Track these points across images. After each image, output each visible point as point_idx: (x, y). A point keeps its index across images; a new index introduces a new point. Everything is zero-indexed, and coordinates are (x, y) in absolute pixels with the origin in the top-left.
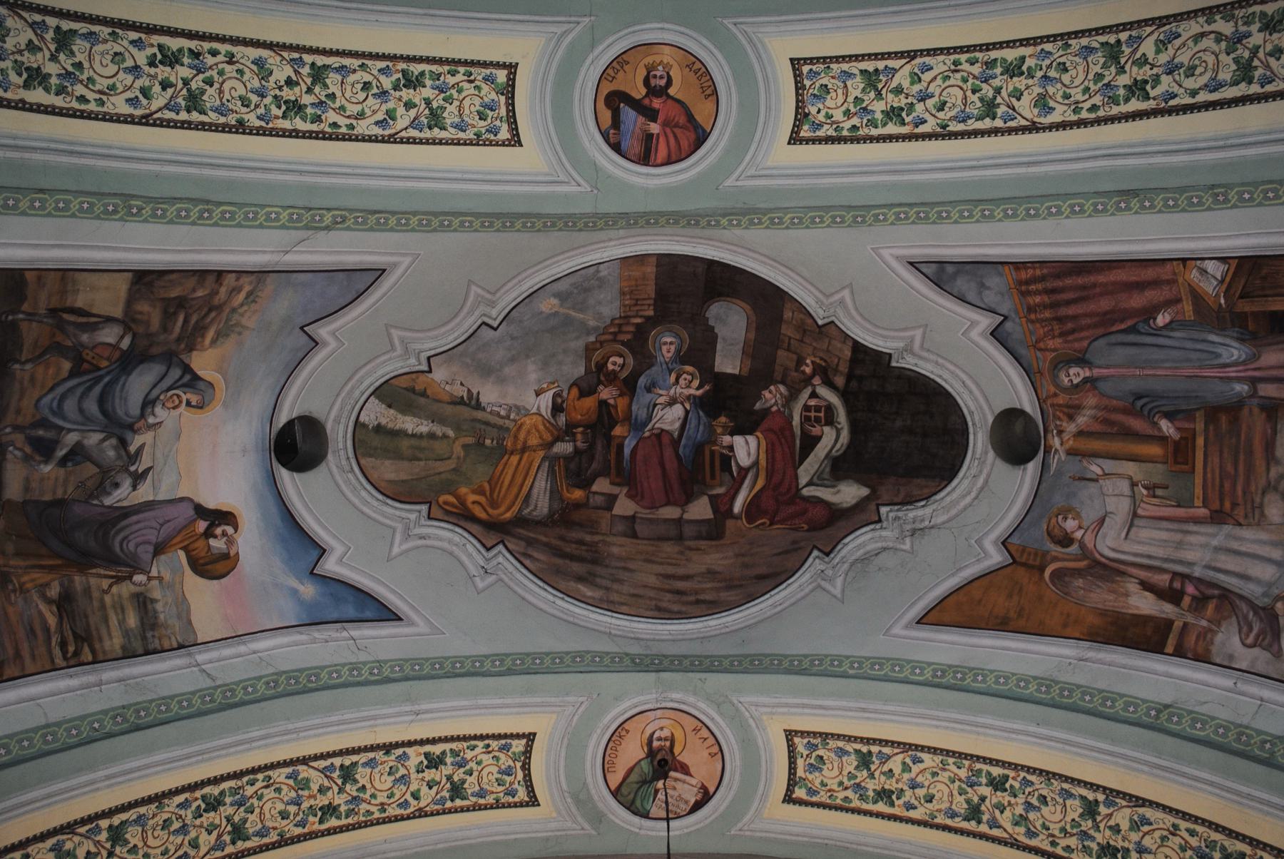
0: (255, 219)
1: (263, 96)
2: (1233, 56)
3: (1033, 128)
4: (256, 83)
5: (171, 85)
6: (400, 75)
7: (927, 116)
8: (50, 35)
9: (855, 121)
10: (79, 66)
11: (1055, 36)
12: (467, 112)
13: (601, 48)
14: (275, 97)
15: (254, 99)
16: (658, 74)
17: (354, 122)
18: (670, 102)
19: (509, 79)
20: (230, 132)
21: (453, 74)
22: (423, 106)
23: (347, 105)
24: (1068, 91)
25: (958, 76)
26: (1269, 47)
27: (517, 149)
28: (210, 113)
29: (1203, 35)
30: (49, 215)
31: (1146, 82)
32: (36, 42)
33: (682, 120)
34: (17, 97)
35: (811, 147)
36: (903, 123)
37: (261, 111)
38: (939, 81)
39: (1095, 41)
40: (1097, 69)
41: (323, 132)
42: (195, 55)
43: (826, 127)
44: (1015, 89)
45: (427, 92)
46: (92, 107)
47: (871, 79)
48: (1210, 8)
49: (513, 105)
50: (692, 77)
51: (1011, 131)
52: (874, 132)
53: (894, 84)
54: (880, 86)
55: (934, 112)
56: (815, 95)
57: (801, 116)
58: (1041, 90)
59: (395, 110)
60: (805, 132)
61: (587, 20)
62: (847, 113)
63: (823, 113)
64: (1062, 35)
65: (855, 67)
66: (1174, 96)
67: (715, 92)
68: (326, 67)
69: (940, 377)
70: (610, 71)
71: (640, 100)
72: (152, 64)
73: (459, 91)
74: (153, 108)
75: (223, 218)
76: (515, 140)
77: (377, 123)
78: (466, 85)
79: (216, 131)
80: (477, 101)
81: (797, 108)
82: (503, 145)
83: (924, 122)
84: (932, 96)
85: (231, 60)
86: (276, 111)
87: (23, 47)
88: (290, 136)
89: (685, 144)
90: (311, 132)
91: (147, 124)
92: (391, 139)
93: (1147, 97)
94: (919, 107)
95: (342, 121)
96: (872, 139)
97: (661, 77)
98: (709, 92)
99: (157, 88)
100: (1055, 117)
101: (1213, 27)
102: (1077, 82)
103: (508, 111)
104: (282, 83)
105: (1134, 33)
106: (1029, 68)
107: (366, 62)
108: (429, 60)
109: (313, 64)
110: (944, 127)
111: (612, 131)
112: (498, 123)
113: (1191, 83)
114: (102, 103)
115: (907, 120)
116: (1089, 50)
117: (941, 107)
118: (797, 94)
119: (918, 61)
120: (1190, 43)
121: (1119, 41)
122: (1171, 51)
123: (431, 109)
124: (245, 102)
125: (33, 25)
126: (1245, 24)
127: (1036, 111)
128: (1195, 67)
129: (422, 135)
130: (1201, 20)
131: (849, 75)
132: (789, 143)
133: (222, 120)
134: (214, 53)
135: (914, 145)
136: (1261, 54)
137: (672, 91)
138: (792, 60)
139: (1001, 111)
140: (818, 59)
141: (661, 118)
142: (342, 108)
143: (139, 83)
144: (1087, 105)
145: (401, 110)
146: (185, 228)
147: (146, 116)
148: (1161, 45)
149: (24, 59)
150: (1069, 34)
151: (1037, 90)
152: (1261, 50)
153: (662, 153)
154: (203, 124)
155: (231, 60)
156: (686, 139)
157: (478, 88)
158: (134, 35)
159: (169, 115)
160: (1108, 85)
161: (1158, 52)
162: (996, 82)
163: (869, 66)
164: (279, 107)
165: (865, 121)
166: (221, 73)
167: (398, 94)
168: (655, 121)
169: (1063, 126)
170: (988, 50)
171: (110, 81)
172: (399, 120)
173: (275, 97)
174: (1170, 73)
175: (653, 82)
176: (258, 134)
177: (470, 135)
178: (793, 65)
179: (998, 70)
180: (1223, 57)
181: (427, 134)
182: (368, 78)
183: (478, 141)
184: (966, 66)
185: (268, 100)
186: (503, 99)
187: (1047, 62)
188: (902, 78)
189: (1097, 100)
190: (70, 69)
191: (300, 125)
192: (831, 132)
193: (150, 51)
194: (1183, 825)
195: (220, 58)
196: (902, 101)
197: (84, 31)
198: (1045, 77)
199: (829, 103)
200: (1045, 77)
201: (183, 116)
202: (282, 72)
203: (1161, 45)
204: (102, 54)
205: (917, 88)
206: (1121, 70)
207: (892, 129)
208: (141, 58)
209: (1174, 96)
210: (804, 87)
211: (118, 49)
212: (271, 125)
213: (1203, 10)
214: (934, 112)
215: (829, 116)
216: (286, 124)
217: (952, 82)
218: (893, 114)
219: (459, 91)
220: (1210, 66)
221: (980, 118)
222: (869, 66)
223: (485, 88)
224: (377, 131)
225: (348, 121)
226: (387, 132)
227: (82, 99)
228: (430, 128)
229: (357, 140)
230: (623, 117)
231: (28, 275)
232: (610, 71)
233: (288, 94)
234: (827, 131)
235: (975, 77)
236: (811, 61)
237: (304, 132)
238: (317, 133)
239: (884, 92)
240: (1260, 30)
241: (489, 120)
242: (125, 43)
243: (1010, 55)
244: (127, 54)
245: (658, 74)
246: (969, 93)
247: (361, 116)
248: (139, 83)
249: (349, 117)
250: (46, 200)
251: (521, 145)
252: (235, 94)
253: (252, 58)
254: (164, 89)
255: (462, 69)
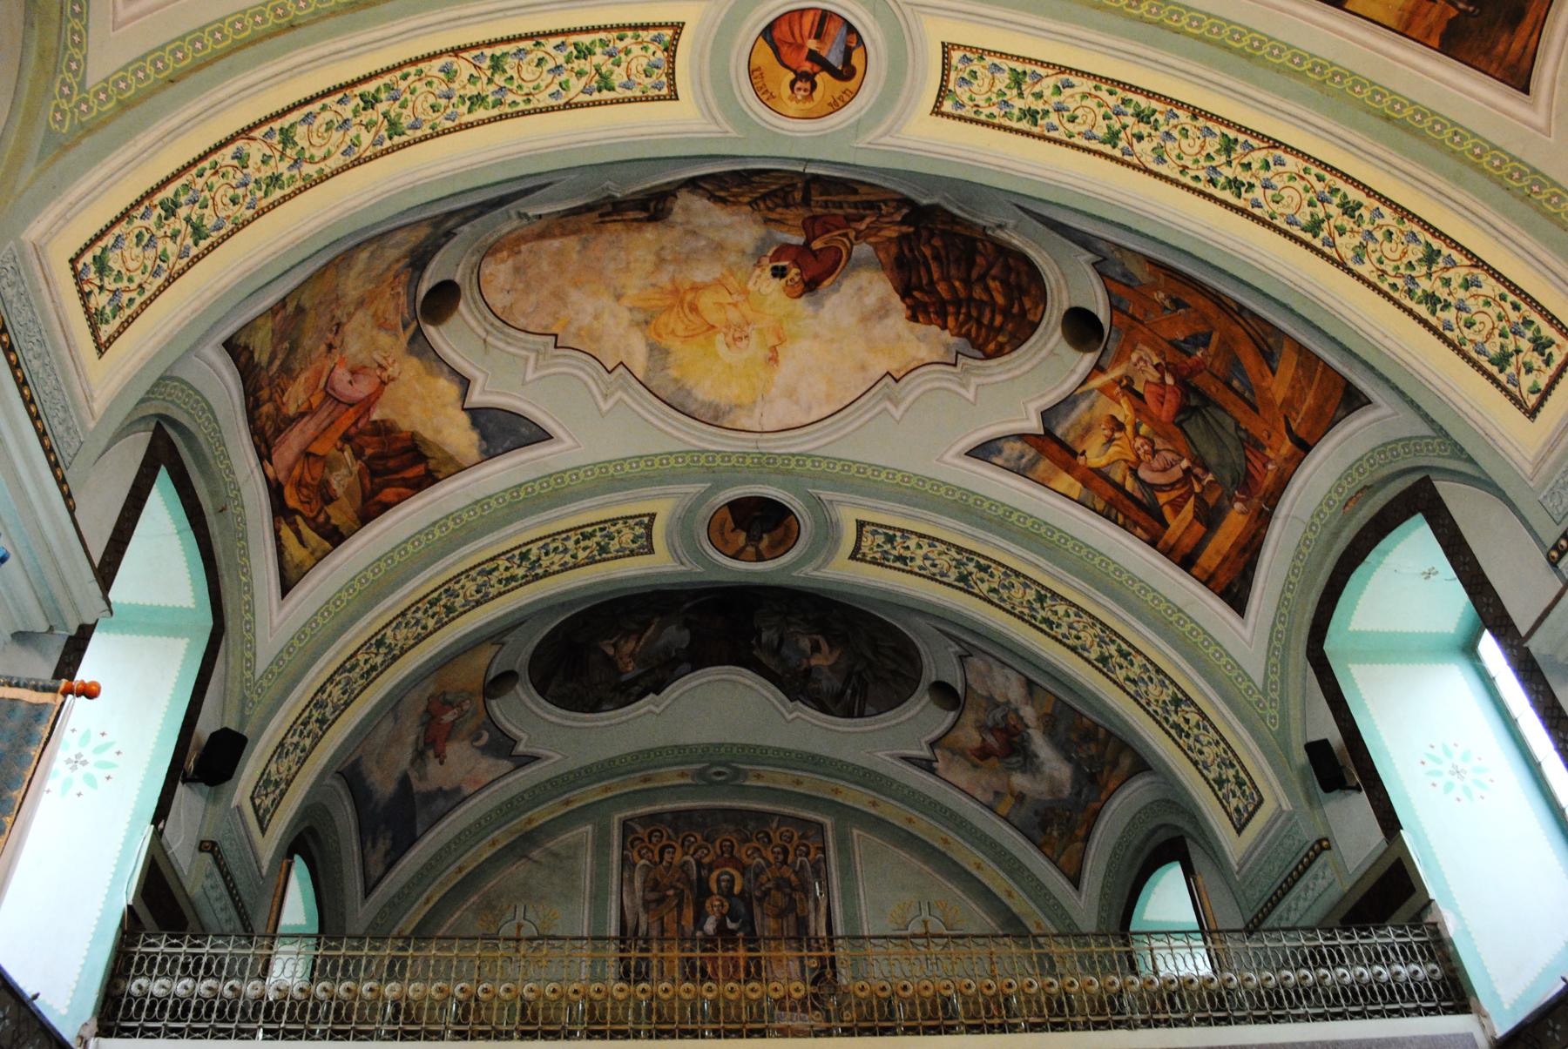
0: (1213, 25)
1: (1168, 134)
2: (299, 148)
3: (456, 51)
4: (1169, 145)
5: (1243, 165)
6: (1040, 122)
7: (553, 52)
8: (1323, 234)
9: (620, 45)
10: (1311, 204)
11: (444, 134)
12: (987, 81)
13: (852, 120)
14: (1156, 129)
15: (1175, 133)
16: (802, 92)
17: (1093, 92)
18: (794, 67)
19: (941, 103)
20: (1207, 112)
21: (992, 115)
22: (1025, 94)
23: (1095, 108)
24: (429, 89)
25: (526, 90)
26: (272, 162)
27: (946, 40)
28: (1218, 133)
29: (325, 158)
30: (1392, 93)
31: (364, 109)
32: (1336, 234)
33: (784, 49)
34: (1372, 200)
35: (663, 20)
36: (576, 45)
37: (1173, 122)
38: (543, 85)
39: (411, 135)
40: (405, 112)
41: (1124, 89)
42: (1212, 182)
43: (648, 39)
44: (474, 84)
45: (1019, 104)
46: (1314, 170)
47: (605, 84)
48: (322, 181)
49: (942, 79)
50: (770, 86)
51: (477, 46)
52: (602, 35)
53: (584, 80)
54: (597, 77)
55: (547, 57)
56: (657, 67)
57: (671, 49)
58: (451, 85)
59: (1053, 94)
60: (667, 34)
61: (860, 145)
62: (627, 52)
63: (650, 51)
64: (438, 135)
65: (620, 93)
66: (340, 102)
67: (750, 73)
68: (1104, 142)
69: (1048, 323)
70: (847, 99)
71: (822, 70)
72: (1251, 186)
73: (989, 99)
74: (1265, 152)
75: (1242, 35)
76: (947, 48)
77: (1072, 86)
78: (982, 103)
79: (1218, 117)
80: (975, 88)
81: (674, 57)
82: (959, 46)
83: (557, 47)
84: (550, 71)
85: (1184, 169)
86: (1161, 118)
87: (1348, 234)
88: (1155, 94)
89: (785, 28)
90: (1135, 92)
91: (1276, 141)
92: (1063, 69)
93: (362, 96)
94: (561, 60)
95: (1104, 95)
96: (605, 29)
97: (799, 89)
98: (756, 73)
99: (1255, 166)
100: (438, 63)
101: (317, 167)
102: (421, 98)
103: (948, 76)
104: (1146, 139)
105: (379, 148)
106: (464, 103)
107: (1067, 139)
108: (1011, 130)
109: (1114, 147)
110: (538, 44)
111: (853, 45)
112: (960, 66)
113: (328, 116)
114: (1305, 170)
115: (572, 48)
116: (414, 127)
117: (540, 61)
118: (673, 69)
119: (562, 101)
120: (333, 149)
121: (390, 138)
122: (348, 139)
123: (1019, 88)
124: (1185, 133)
125: (1333, 245)
126: (293, 177)
127: (455, 67)
128: (327, 130)
129: (1034, 68)
130: (327, 171)
131: (626, 86)
132: (683, 24)
133: (1210, 124)
134: (1197, 178)
135: (565, 26)
136: (277, 155)
137: (792, 76)
138: (677, 99)
139: (486, 64)
140: (653, 100)
141: (805, 52)
142: (1100, 105)
143: (1268, 175)
144: (412, 78)
145: (1047, 93)
146: (1280, 37)
147: (1274, 147)
148: (355, 143)
149: (1352, 225)
150: (432, 137)
151: (455, 86)
152: (278, 158)
153: (808, 20)
154: (1228, 126)
155: (1184, 169)
156: (782, 32)
157: (971, 99)
158: (1257, 211)
159: (1254, 142)
160: (395, 99)
161: (358, 137)
162: (492, 88)
163: (606, 95)
164: (1156, 121)
165: (611, 45)
166: (1197, 161)
167: (1046, 107)
168: (810, 51)
169: (430, 57)
170: (501, 116)
171: (1292, 184)
172: (1051, 86)
173: (1156, 129)
174: (346, 121)
175: (808, 85)
176: (1183, 103)
177: (989, 60)
178: (676, 95)
179: (491, 99)
180: (305, 144)
181: (1029, 68)
182: (1070, 126)
183: (982, 53)
184: (519, 99)
185: (1163, 129)
186: (951, 87)
187: (448, 111)
188: (576, 85)
189: (403, 85)
190: (1319, 204)
191: (1143, 102)
192: (643, 34)
193: (1249, 196)
194: (1222, 745)
195: (1193, 173)
196: (578, 65)
197: (1295, 227)
198: (449, 98)
199: (644, 62)
200: (449, 98)
201: (1242, 138)
202: (1144, 150)
203: (355, 143)
204: (1288, 206)
205: (564, 77)
206: (385, 115)
207: (585, 39)
208: (1258, 193)
209: (340, 102)
210: (667, 75)
211: (1274, 206)
212: (1169, 108)
213: (328, 178)
214: (547, 57)
215: (645, 49)
216: (1154, 104)
217: (531, 85)
218: (584, 53)
219: (989, 99)
220: (315, 135)
221: (505, 55)
222: (606, 95)
223: (965, 98)
224: (1074, 79)
225: (1099, 93)
226: (1065, 76)
227: (1320, 179)
228: (1025, 73)
229: (1095, 76)
230: (841, 56)
231: (1435, 42)
232: (847, 99)
233: (1145, 129)
234: (646, 35)
235: (511, 91)
236: (659, 98)
237: (1141, 93)
238: (1130, 90)
239: (594, 72)
240: (281, 174)
241: (968, 70)
242: (1266, 208)
243: (481, 113)
244: (1269, 199)
245: (802, 92)
246: (516, 76)
247: (1085, 96)
248: (1268, 175)
249: (1096, 97)
250: (1389, 108)
251: (943, 43)
252: (1190, 141)
253: (1165, 166)
254: (1250, 164)
255: (983, 117)
